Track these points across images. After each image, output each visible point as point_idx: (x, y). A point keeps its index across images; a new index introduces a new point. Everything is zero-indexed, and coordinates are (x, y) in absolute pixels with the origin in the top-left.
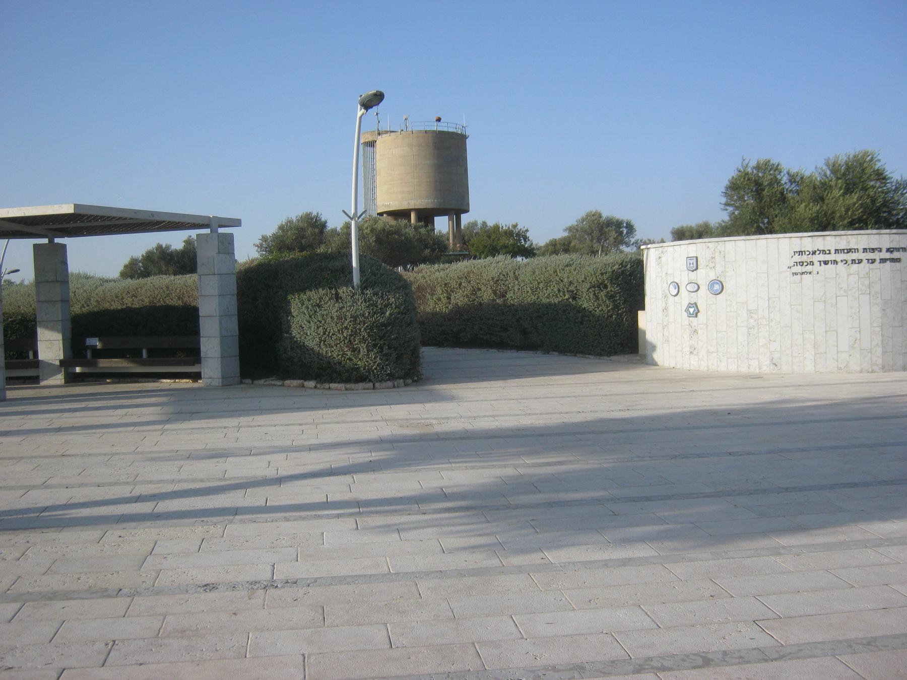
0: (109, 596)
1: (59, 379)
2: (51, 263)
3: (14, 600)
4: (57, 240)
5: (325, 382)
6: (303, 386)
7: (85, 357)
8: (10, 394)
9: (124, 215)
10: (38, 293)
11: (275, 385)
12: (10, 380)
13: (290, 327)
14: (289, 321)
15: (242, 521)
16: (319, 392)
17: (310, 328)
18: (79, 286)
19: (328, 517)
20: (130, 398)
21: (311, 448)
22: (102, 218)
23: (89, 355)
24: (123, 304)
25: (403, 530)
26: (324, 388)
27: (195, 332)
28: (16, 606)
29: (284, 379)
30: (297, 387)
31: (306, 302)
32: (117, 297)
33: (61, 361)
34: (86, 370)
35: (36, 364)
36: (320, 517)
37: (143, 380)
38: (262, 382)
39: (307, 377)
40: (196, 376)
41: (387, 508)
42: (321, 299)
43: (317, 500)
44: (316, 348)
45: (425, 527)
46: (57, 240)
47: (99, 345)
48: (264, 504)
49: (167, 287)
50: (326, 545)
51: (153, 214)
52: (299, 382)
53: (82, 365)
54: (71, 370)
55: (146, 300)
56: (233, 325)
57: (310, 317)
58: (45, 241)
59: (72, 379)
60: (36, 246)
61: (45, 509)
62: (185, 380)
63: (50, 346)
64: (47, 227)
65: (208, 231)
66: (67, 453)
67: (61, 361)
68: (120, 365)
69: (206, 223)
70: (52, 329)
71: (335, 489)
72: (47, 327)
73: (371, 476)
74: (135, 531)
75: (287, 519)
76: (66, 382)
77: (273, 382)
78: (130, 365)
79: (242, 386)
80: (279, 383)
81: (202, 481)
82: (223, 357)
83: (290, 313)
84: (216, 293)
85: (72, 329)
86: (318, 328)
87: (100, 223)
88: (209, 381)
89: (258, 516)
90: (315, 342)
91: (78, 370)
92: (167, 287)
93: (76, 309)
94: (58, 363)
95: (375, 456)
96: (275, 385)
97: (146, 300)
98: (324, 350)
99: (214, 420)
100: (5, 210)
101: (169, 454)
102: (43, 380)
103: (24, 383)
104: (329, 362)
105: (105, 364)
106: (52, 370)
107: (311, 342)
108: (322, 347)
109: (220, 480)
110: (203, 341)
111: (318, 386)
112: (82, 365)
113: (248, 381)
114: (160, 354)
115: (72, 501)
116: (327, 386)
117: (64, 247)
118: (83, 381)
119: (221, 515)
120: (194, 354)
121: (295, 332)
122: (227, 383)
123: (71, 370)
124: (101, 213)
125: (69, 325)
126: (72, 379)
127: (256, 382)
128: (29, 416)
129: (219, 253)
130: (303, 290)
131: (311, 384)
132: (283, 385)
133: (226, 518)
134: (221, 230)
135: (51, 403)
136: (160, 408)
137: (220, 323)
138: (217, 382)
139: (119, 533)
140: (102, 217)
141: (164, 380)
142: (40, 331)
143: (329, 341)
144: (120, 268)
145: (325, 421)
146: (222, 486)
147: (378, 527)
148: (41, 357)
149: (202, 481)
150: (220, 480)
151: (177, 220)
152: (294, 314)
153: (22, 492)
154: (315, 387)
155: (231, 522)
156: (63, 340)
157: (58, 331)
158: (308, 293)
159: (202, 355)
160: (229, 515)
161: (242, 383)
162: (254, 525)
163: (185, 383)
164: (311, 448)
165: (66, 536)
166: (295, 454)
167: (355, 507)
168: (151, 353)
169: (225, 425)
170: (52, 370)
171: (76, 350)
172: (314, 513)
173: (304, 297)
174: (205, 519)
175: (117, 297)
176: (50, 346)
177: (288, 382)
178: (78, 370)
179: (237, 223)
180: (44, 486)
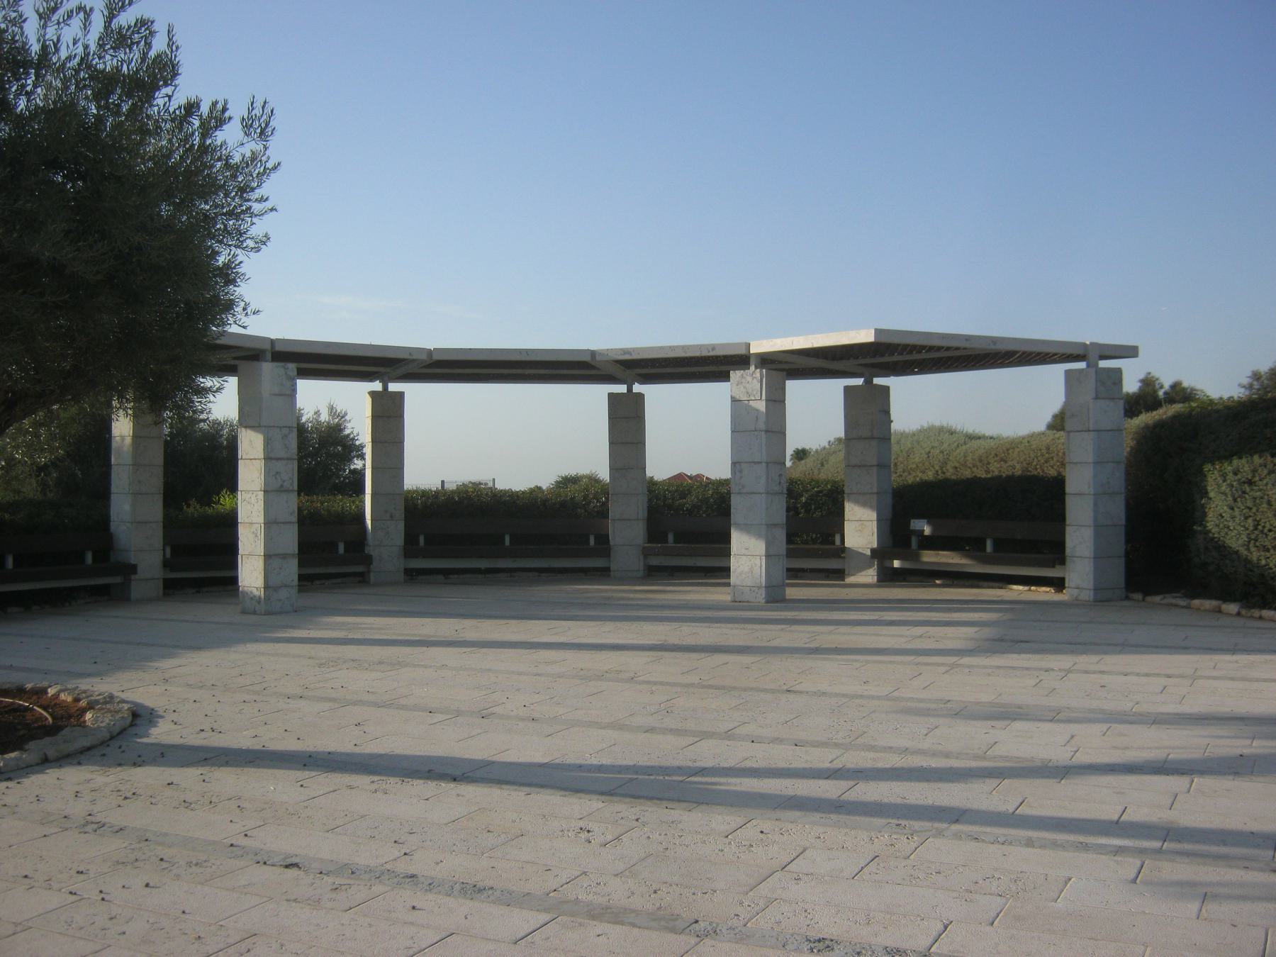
0: (673, 930)
1: (869, 575)
2: (868, 413)
3: (546, 910)
4: (877, 381)
5: (1254, 607)
6: (1220, 611)
7: (908, 545)
8: (792, 593)
9: (954, 344)
10: (848, 454)
11: (1176, 606)
12: (794, 573)
13: (1205, 514)
14: (1203, 506)
15: (957, 836)
16: (1239, 622)
17: (1233, 518)
18: (936, 444)
19: (1101, 849)
20: (949, 610)
21: (1158, 720)
22: (931, 349)
23: (914, 542)
24: (987, 472)
25: (1216, 897)
26: (1252, 617)
27: (1060, 518)
28: (545, 917)
29: (1193, 597)
30: (1209, 611)
31: (1230, 476)
32: (981, 461)
33: (873, 550)
34: (908, 565)
35: (841, 551)
36: (1085, 847)
37: (986, 584)
38: (1157, 599)
39: (1226, 597)
40: (1059, 584)
41: (1214, 849)
42: (1254, 471)
43: (1104, 817)
44: (1244, 552)
45: (1259, 899)
46: (877, 381)
47: (927, 530)
48: (1011, 811)
49: (1048, 448)
50: (1060, 904)
51: (994, 340)
52: (1214, 603)
53: (901, 559)
54: (887, 564)
55: (1018, 467)
56: (1117, 509)
57: (1235, 500)
58: (859, 381)
59: (889, 577)
60: (847, 389)
61: (702, 771)
62: (1044, 589)
63: (861, 528)
64: (861, 361)
65: (1082, 365)
66: (797, 688)
67: (873, 550)
68: (951, 561)
69: (1081, 352)
70: (865, 504)
71: (1147, 800)
72: (857, 502)
73: (1227, 783)
74: (790, 826)
75: (1029, 843)
76: (879, 580)
77: (1174, 601)
78: (964, 561)
79: (1126, 603)
80: (1182, 602)
81: (947, 755)
82: (1097, 558)
83: (1207, 493)
84: (1091, 458)
85: (894, 506)
86: (1246, 518)
87: (924, 355)
88: (1076, 592)
89: (988, 829)
90: (1240, 542)
91: (896, 564)
92: (1048, 448)
93: (896, 480)
94: (869, 553)
95: (1259, 746)
96: (1176, 606)
97: (1018, 467)
98: (1255, 555)
99: (1038, 657)
100: (789, 339)
101: (933, 706)
102: (850, 575)
103: (827, 578)
104: (1263, 575)
105: (931, 558)
106: (861, 562)
107: (1235, 540)
108: (1253, 549)
109: (976, 757)
110: (1069, 531)
111: (1243, 612)
112: (901, 559)
113: (1138, 596)
114: (1011, 548)
115: (748, 764)
116: (1256, 613)
117: (886, 389)
118: (904, 580)
119: (931, 819)
120: (1055, 551)
121: (1211, 523)
122: (1102, 597)
123: (887, 564)
124: (896, 340)
125: (888, 500)
126: (889, 577)
127: (1149, 599)
128: (794, 627)
129: (1097, 398)
130: (1228, 457)
131: (1232, 608)
132: (1188, 607)
133: (936, 825)
134: (1103, 364)
135: (908, 610)
136: (976, 629)
137: (1095, 505)
138: (1088, 595)
139: (766, 826)
140: (923, 347)
141: (1015, 587)
142: (849, 507)
143: (1263, 541)
144: (1048, 418)
145: (1215, 674)
146: (970, 769)
147: (1181, 884)
148: (849, 543)
149: (947, 755)
150: (976, 757)
151: (1002, 347)
152: (1212, 495)
153: (692, 740)
154: (1238, 614)
155: (940, 833)
156: (879, 520)
157: (871, 507)
158: (1235, 462)
159: (1068, 551)
160: (940, 820)
161: (1127, 598)
162: (974, 844)
163: (1044, 593)
164: (1158, 720)
165: (692, 819)
166: (1121, 727)
167: (1156, 838)
168: (999, 545)
169: (1051, 665)
170: (861, 562)
171: (896, 537)
172: (1081, 838)
173: (1228, 468)
174: (903, 822)
175: (981, 461)
176: (861, 528)
177: (1196, 602)
178: (896, 564)
179: (1130, 352)
180: (729, 735)
